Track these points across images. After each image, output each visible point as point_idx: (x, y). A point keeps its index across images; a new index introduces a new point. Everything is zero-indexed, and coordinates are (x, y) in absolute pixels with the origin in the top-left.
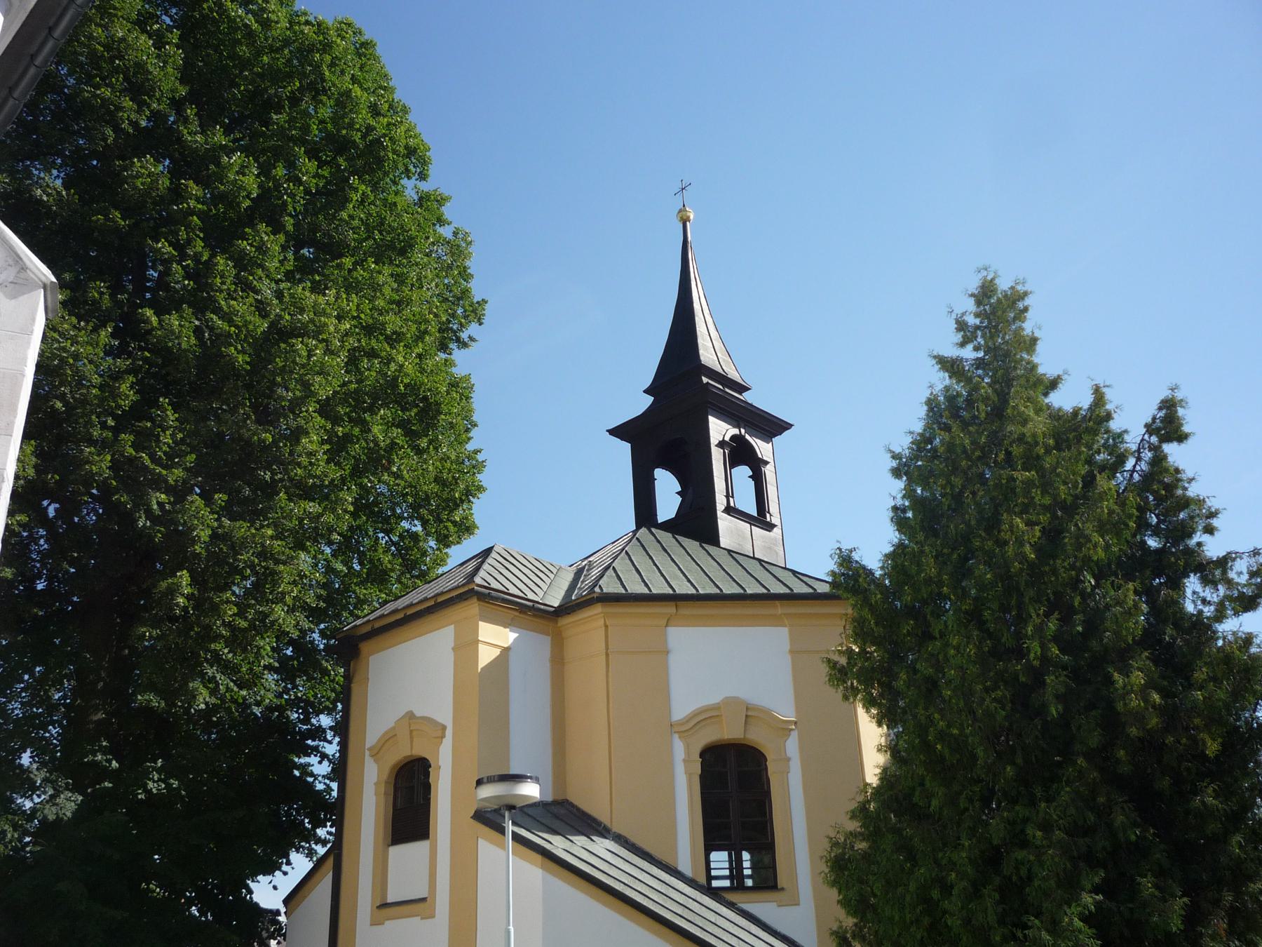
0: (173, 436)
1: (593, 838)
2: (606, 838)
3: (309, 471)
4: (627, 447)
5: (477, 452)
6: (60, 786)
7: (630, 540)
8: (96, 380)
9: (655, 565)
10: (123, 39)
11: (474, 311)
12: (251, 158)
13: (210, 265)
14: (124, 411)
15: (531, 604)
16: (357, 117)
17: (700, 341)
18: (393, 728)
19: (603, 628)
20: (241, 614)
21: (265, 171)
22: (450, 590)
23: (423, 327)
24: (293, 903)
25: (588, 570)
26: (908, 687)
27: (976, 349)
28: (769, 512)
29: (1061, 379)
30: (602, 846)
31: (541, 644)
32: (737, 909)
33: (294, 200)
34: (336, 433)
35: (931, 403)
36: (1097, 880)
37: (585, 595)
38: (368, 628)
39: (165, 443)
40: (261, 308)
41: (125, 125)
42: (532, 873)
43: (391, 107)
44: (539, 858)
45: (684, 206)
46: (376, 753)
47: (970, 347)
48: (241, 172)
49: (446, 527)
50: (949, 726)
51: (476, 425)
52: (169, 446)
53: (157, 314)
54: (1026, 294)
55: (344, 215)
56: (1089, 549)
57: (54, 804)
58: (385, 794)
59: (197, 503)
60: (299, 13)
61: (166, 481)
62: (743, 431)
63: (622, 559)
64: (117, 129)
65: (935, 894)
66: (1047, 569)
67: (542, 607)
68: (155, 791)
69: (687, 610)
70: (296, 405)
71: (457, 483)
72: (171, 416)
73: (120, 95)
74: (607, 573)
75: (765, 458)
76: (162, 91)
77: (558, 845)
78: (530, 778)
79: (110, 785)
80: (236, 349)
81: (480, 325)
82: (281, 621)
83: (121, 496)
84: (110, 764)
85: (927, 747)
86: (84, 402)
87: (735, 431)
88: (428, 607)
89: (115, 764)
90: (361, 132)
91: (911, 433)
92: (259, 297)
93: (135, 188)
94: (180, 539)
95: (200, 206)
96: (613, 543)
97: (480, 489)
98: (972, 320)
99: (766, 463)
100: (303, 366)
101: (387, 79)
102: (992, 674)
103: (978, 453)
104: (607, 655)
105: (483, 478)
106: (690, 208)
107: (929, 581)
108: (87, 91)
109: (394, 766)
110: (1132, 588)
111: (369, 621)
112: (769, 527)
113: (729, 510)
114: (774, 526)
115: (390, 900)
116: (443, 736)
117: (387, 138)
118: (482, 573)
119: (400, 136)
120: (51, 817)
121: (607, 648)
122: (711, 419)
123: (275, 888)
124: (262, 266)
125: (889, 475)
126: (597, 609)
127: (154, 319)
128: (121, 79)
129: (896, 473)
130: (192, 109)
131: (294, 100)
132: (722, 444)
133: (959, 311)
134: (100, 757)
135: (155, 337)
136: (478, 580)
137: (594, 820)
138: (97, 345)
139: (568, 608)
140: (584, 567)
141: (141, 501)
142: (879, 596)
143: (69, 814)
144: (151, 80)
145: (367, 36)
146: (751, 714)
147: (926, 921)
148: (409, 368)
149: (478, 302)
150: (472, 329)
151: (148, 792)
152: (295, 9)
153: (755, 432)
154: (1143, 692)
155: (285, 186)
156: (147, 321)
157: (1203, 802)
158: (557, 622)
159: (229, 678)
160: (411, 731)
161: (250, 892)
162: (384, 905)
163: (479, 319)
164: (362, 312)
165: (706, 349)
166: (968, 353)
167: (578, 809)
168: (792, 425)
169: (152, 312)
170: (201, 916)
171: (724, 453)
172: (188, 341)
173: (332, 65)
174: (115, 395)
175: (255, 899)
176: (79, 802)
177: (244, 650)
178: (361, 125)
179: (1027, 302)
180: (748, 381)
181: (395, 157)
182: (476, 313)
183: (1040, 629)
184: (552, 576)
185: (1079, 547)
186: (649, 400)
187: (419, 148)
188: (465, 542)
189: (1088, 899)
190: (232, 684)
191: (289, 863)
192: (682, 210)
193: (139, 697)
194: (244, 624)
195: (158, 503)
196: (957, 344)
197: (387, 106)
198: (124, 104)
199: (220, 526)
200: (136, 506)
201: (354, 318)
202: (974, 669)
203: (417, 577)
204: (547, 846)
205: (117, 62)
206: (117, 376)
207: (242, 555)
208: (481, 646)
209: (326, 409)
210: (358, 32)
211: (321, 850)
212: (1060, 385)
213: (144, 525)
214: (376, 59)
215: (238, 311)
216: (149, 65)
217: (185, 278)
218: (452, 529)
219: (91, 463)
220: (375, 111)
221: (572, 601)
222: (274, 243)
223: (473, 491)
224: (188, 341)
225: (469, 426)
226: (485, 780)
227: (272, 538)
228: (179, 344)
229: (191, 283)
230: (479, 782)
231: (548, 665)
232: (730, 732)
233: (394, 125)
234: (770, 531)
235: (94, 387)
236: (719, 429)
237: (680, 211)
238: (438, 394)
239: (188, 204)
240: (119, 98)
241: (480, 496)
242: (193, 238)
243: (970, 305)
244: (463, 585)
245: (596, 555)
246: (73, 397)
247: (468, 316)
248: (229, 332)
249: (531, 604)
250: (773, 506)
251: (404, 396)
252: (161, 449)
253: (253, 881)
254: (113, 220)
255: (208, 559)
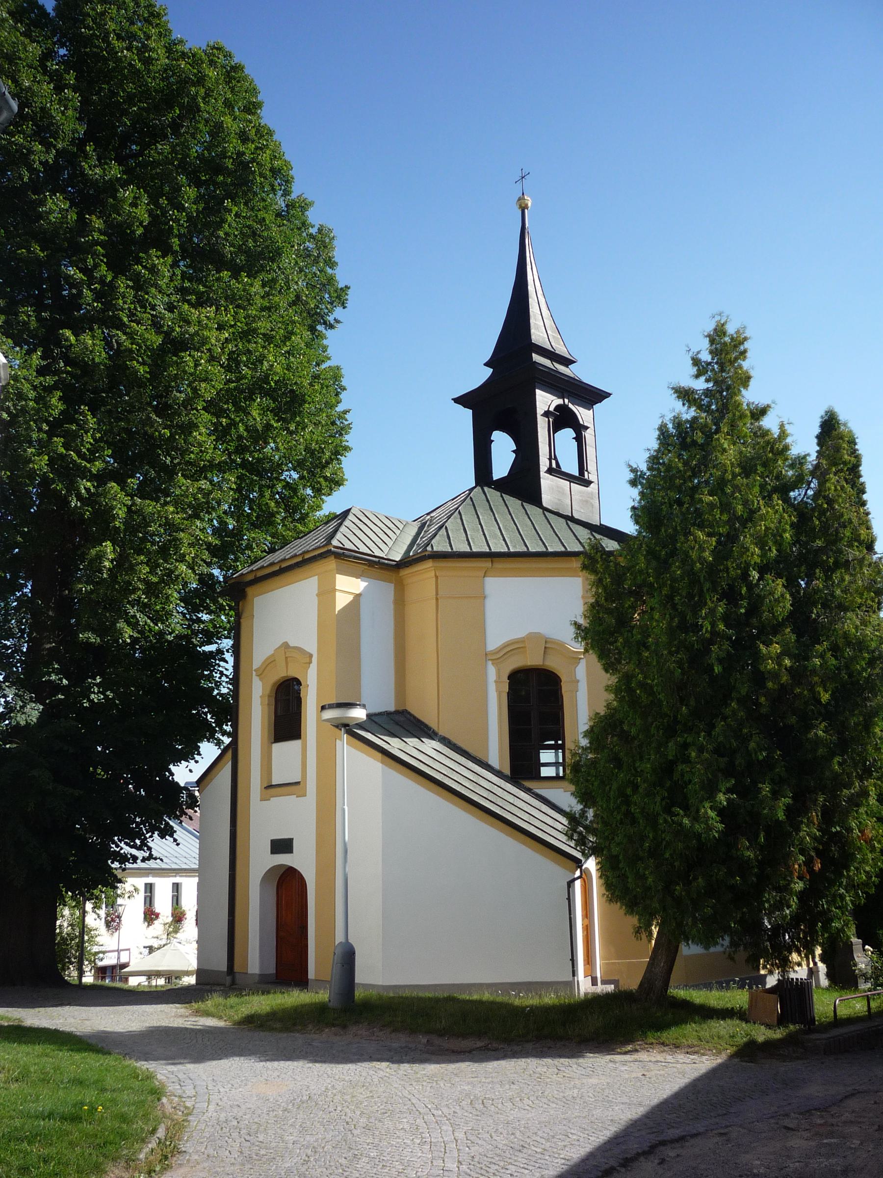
0: (93, 436)
1: (423, 739)
2: (434, 739)
3: (201, 456)
4: (469, 413)
5: (346, 412)
6: (27, 699)
7: (465, 500)
8: (32, 394)
9: (480, 524)
10: (30, 88)
11: (339, 297)
12: (142, 190)
13: (112, 286)
14: (54, 418)
15: (377, 560)
16: (229, 146)
17: (532, 321)
18: (273, 655)
19: (434, 579)
20: (152, 572)
21: (154, 200)
22: (314, 549)
23: (290, 328)
24: (202, 784)
25: (429, 526)
26: (624, 648)
27: (707, 381)
28: (587, 471)
29: (770, 407)
30: (430, 746)
31: (386, 590)
32: (533, 793)
33: (177, 222)
34: (221, 423)
35: (663, 429)
36: (728, 785)
37: (420, 552)
38: (251, 577)
39: (87, 442)
40: (156, 324)
41: (36, 165)
42: (373, 765)
43: (258, 131)
44: (379, 755)
45: (523, 194)
46: (261, 674)
47: (703, 378)
48: (134, 205)
49: (319, 482)
50: (645, 678)
51: (345, 389)
52: (91, 444)
53: (76, 335)
54: (745, 339)
55: (221, 234)
56: (748, 556)
57: (23, 713)
58: (268, 704)
59: (115, 489)
60: (176, 42)
61: (90, 471)
62: (566, 401)
63: (455, 518)
64: (31, 169)
65: (629, 791)
66: (722, 567)
67: (386, 561)
68: (96, 700)
69: (500, 564)
70: (188, 403)
71: (323, 452)
72: (92, 421)
73: (31, 140)
74: (440, 533)
75: (585, 424)
76: (64, 133)
77: (394, 745)
78: (359, 705)
79: (63, 697)
80: (138, 362)
81: (344, 308)
82: (183, 575)
83: (57, 485)
84: (62, 681)
85: (631, 691)
86: (24, 411)
87: (560, 401)
88: (297, 563)
89: (65, 682)
90: (233, 158)
91: (648, 450)
92: (155, 313)
93: (50, 223)
94: (104, 515)
95: (102, 237)
96: (453, 499)
97: (347, 449)
98: (706, 357)
99: (587, 428)
100: (191, 374)
101: (256, 93)
102: (676, 642)
103: (689, 473)
104: (437, 599)
105: (350, 439)
106: (528, 196)
107: (641, 572)
108: (4, 139)
109: (275, 684)
110: (781, 583)
111: (252, 571)
112: (588, 483)
113: (550, 471)
114: (591, 482)
115: (273, 784)
116: (310, 662)
117: (255, 164)
118: (339, 536)
119: (266, 160)
120: (23, 723)
121: (437, 594)
122: (538, 392)
123: (191, 771)
124: (156, 286)
125: (628, 486)
126: (429, 564)
127: (72, 338)
128: (30, 125)
129: (633, 483)
130: (90, 146)
131: (175, 126)
132: (547, 414)
133: (695, 350)
134: (54, 677)
135: (73, 353)
136: (335, 542)
137: (426, 726)
138: (31, 366)
139: (407, 562)
140: (425, 523)
141: (72, 487)
142: (608, 580)
143: (35, 720)
144: (55, 123)
145: (236, 60)
146: (549, 646)
147: (624, 808)
148: (278, 368)
149: (341, 289)
150: (338, 313)
151: (91, 701)
152: (173, 38)
153: (578, 401)
154: (779, 658)
155: (171, 212)
156: (67, 340)
157: (816, 734)
158: (398, 573)
159: (146, 615)
160: (286, 658)
161: (172, 774)
162: (270, 786)
163: (343, 303)
164: (239, 321)
165: (537, 328)
166: (700, 385)
167: (414, 717)
168: (610, 394)
169: (70, 332)
170: (136, 792)
171: (549, 421)
172: (100, 356)
173: (207, 95)
174: (47, 406)
175: (176, 780)
176: (41, 710)
177: (157, 597)
178: (232, 153)
179: (747, 345)
180: (575, 355)
181: (262, 179)
182: (340, 297)
183: (713, 611)
184: (398, 532)
185: (742, 554)
186: (489, 371)
187: (283, 169)
188: (334, 494)
189: (722, 798)
190: (149, 621)
191: (199, 754)
192: (521, 199)
193: (81, 636)
194: (155, 579)
195: (85, 488)
196: (693, 376)
197: (254, 131)
198: (35, 148)
199: (134, 504)
200: (69, 491)
201: (232, 326)
202: (664, 639)
203: (298, 521)
204: (385, 746)
205: (26, 110)
206: (49, 390)
207: (151, 526)
208: (337, 594)
209: (212, 407)
210: (228, 55)
211: (227, 740)
212: (769, 413)
213: (76, 505)
214: (245, 79)
215: (138, 331)
216: (53, 111)
217: (94, 301)
218: (324, 483)
219: (33, 462)
220: (244, 137)
221: (409, 557)
222: (163, 264)
223: (339, 451)
224: (100, 356)
225: (339, 390)
226: (327, 707)
227: (173, 513)
228: (93, 359)
229: (99, 304)
230: (323, 708)
231: (392, 606)
232: (533, 659)
233: (261, 149)
234: (587, 487)
235: (31, 400)
236: (545, 401)
237: (519, 199)
238: (302, 387)
239: (93, 236)
240: (30, 142)
241: (347, 454)
242: (98, 263)
243: (705, 344)
244: (323, 546)
245: (442, 508)
246: (15, 409)
247: (334, 301)
248: (132, 348)
249: (377, 560)
250: (591, 466)
251: (275, 390)
252: (84, 447)
253: (174, 765)
254: (33, 252)
255: (125, 530)
